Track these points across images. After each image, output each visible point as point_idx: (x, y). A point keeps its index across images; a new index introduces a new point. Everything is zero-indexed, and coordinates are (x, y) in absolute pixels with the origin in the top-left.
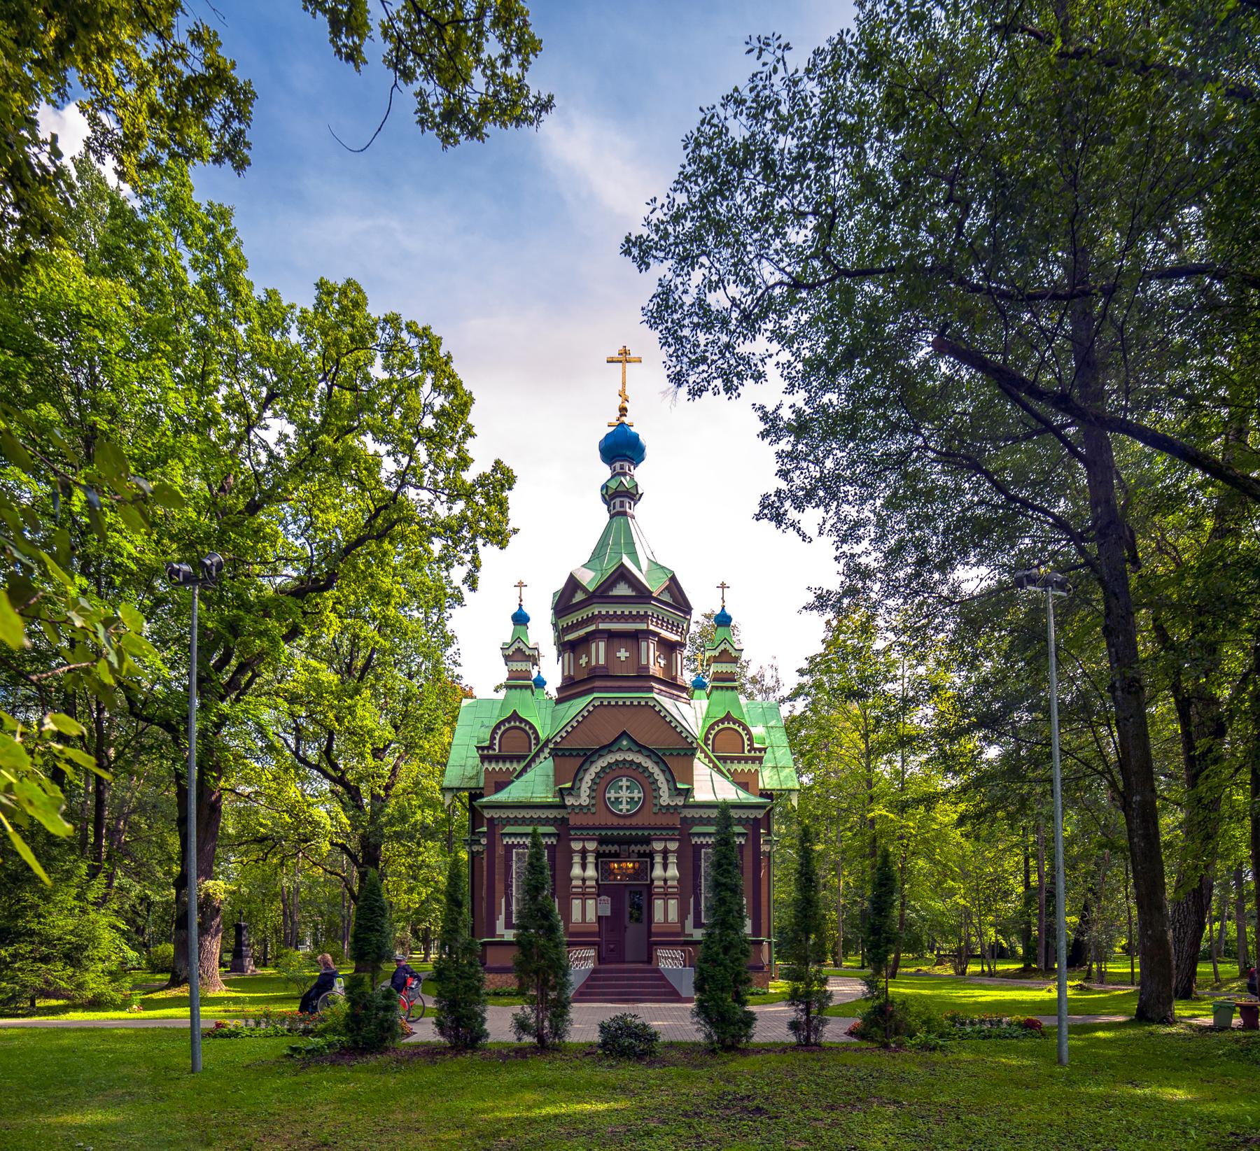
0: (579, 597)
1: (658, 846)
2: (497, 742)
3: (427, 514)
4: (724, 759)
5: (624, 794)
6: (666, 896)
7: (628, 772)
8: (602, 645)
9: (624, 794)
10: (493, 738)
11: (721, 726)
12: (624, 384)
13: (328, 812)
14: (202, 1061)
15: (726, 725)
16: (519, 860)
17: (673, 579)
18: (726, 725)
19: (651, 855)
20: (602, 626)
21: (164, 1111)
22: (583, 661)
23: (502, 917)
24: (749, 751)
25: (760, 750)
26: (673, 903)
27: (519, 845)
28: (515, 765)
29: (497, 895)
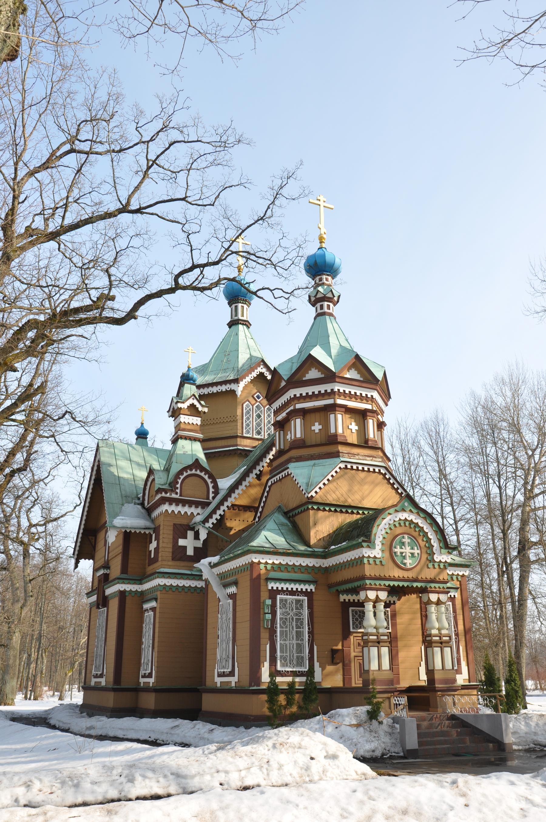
5: (407, 550)
7: (409, 531)
8: (298, 421)
9: (407, 550)
11: (189, 472)
12: (192, 6)
14: (267, 615)
15: (194, 472)
18: (194, 472)
19: (361, 604)
20: (298, 406)
23: (267, 664)
27: (282, 591)
28: (199, 510)
29: (263, 641)
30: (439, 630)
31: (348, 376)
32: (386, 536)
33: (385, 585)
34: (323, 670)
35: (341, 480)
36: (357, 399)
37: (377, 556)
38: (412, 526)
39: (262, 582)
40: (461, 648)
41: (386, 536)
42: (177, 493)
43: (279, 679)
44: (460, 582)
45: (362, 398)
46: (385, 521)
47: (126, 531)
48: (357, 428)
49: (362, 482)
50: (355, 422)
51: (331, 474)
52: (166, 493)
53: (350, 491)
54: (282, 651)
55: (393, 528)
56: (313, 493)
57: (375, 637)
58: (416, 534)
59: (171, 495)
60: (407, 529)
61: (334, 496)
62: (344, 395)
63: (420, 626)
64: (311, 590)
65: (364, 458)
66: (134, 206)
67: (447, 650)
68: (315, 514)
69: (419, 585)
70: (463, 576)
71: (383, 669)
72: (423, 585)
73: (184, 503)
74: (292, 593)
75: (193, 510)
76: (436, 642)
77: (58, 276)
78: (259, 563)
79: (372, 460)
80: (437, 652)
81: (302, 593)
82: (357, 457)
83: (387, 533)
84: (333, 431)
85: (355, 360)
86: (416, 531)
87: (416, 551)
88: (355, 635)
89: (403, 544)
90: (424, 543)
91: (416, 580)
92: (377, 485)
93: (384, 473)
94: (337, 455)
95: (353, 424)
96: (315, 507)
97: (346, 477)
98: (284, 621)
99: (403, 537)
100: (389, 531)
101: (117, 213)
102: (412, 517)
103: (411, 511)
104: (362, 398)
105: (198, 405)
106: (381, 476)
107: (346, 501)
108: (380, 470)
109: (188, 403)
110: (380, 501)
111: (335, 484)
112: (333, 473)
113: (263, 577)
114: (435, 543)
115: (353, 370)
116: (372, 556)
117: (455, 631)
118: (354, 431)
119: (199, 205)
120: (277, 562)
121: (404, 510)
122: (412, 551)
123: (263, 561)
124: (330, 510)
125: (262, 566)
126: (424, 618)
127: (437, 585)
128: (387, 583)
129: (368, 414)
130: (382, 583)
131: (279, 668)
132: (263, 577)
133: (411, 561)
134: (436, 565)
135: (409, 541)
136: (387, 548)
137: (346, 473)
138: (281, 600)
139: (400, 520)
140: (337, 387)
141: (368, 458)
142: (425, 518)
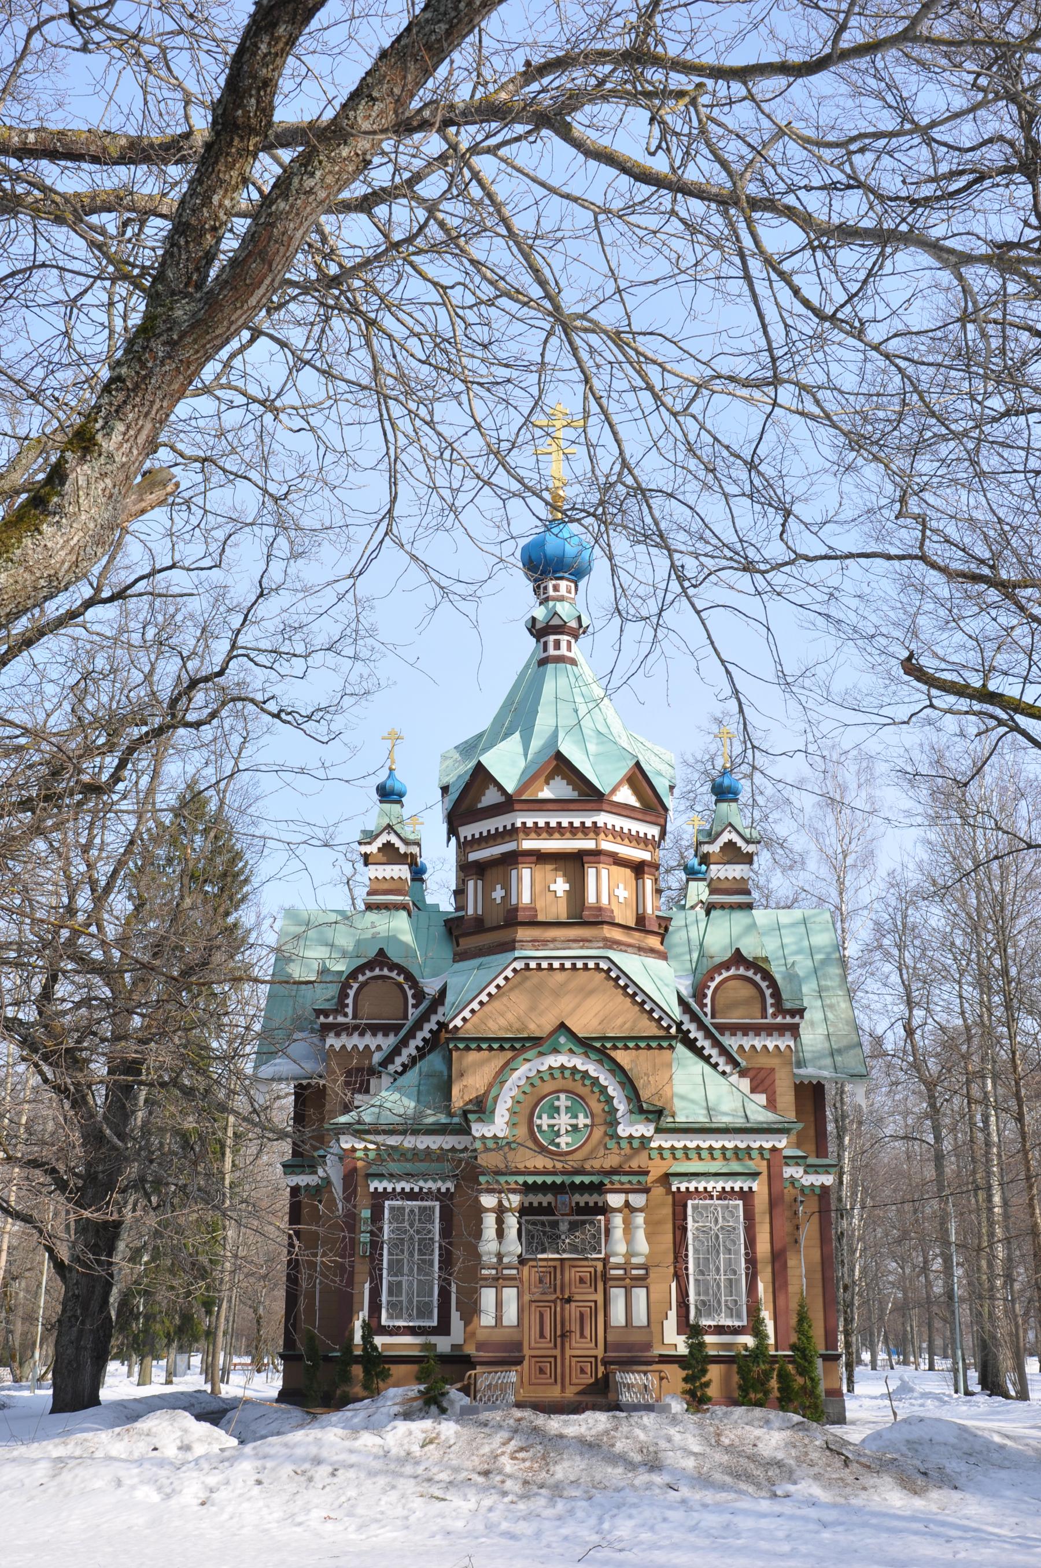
0: (491, 797)
1: (615, 1200)
2: (350, 1001)
4: (722, 1028)
5: (563, 1121)
6: (498, 1282)
9: (563, 1121)
10: (343, 995)
15: (377, 972)
17: (638, 764)
18: (377, 972)
21: (1009, 1279)
22: (498, 894)
23: (673, 1314)
26: (510, 1294)
27: (393, 1195)
31: (546, 794)
32: (521, 1098)
33: (516, 1182)
34: (465, 1326)
35: (517, 991)
36: (562, 835)
37: (501, 1135)
38: (578, 1077)
39: (360, 1180)
40: (761, 1286)
41: (521, 1098)
42: (346, 1015)
43: (379, 1341)
44: (768, 1160)
45: (573, 831)
46: (516, 1074)
47: (802, 1083)
48: (567, 887)
49: (557, 993)
50: (564, 875)
51: (495, 983)
52: (327, 1016)
53: (533, 1008)
54: (390, 1293)
55: (537, 1082)
56: (458, 1022)
57: (621, 1272)
58: (581, 1090)
59: (335, 1018)
60: (560, 1083)
61: (502, 1022)
62: (537, 831)
63: (671, 1246)
64: (448, 1189)
65: (566, 945)
66: (106, 594)
68: (460, 1059)
69: (587, 1180)
70: (774, 1149)
71: (505, 1323)
72: (596, 1179)
73: (362, 1031)
74: (411, 1196)
75: (370, 1041)
78: (354, 1150)
79: (582, 948)
80: (617, 1296)
81: (429, 1195)
82: (551, 945)
83: (524, 1093)
84: (514, 901)
85: (555, 763)
86: (584, 1085)
87: (582, 1121)
88: (531, 1263)
89: (557, 1109)
90: (602, 1105)
92: (591, 992)
93: (606, 968)
94: (509, 946)
95: (560, 880)
96: (461, 1046)
97: (528, 984)
98: (396, 1245)
99: (558, 1099)
100: (528, 1089)
101: (82, 610)
102: (578, 1062)
103: (571, 1051)
104: (573, 831)
106: (603, 975)
107: (525, 1028)
108: (597, 965)
109: (379, 843)
110: (595, 1022)
111: (505, 1000)
112: (500, 981)
113: (361, 1173)
114: (621, 1106)
115: (558, 779)
116: (489, 1135)
117: (747, 1254)
118: (560, 893)
119: (202, 569)
121: (556, 1051)
122: (574, 1121)
124: (491, 1049)
125: (360, 1154)
126: (678, 1232)
127: (625, 1179)
128: (521, 1179)
129: (586, 859)
130: (511, 1179)
131: (384, 1321)
132: (361, 1173)
133: (569, 1140)
134: (624, 1144)
135: (569, 1103)
137: (527, 978)
138: (392, 1209)
139: (550, 1068)
140: (520, 820)
141: (575, 945)
142: (600, 1062)
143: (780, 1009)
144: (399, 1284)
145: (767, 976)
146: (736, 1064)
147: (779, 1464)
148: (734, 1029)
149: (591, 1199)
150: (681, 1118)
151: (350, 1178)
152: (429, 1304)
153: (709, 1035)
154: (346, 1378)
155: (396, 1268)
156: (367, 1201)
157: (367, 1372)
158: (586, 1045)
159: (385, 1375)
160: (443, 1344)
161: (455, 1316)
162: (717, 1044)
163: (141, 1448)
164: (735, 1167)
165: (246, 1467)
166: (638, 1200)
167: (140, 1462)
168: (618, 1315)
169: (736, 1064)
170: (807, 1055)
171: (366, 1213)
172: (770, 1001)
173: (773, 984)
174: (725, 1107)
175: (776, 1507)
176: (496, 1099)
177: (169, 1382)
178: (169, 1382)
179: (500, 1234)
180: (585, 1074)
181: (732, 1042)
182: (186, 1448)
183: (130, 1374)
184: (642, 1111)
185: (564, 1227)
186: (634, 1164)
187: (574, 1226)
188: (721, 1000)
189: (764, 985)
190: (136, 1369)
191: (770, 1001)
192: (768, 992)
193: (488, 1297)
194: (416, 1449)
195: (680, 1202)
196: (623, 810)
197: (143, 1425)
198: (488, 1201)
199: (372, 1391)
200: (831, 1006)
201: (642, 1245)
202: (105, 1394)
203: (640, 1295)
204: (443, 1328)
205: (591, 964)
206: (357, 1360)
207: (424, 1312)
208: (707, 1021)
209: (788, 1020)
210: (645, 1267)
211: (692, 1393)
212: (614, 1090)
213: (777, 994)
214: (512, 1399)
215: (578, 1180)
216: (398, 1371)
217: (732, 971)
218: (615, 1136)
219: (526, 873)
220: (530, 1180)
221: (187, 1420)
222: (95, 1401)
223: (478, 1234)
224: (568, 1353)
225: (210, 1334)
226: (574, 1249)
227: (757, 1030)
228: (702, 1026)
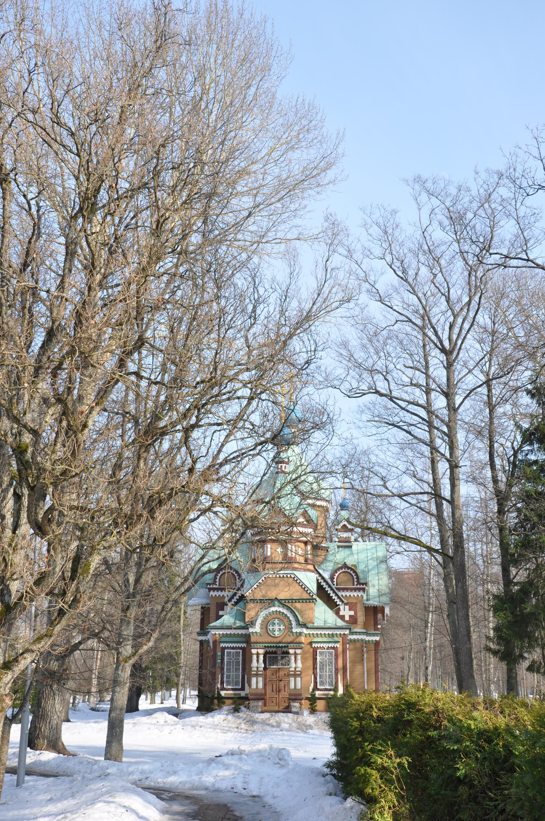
2: (217, 580)
3: (220, 220)
4: (339, 589)
6: (257, 675)
9: (277, 627)
13: (174, 592)
16: (228, 655)
24: (357, 585)
25: (363, 584)
26: (260, 679)
27: (228, 648)
30: (257, 668)
39: (218, 643)
40: (339, 676)
54: (227, 678)
56: (247, 594)
58: (281, 618)
67: (298, 679)
69: (283, 645)
70: (344, 634)
72: (286, 645)
74: (233, 648)
76: (292, 675)
77: (270, 451)
81: (239, 648)
87: (282, 627)
91: (280, 643)
98: (229, 663)
102: (281, 609)
105: (348, 525)
109: (342, 524)
114: (294, 623)
120: (221, 633)
121: (274, 606)
123: (217, 633)
125: (217, 636)
128: (264, 645)
130: (261, 645)
136: (264, 627)
143: (359, 583)
144: (230, 675)
145: (355, 572)
146: (343, 602)
147: (310, 726)
148: (344, 589)
149: (285, 650)
150: (316, 625)
151: (215, 642)
152: (238, 682)
153: (334, 592)
154: (212, 703)
155: (229, 670)
156: (220, 650)
157: (218, 702)
158: (282, 603)
159: (224, 703)
160: (243, 694)
161: (246, 685)
162: (337, 595)
163: (154, 721)
164: (331, 640)
165: (179, 726)
166: (298, 651)
167: (154, 724)
168: (292, 686)
169: (343, 602)
170: (371, 597)
171: (219, 654)
172: (355, 580)
173: (357, 574)
174: (329, 621)
175: (306, 735)
176: (256, 620)
177: (162, 703)
178: (162, 703)
179: (258, 661)
180: (283, 613)
181: (340, 594)
182: (166, 722)
183: (146, 699)
184: (300, 624)
185: (279, 658)
186: (298, 640)
187: (282, 658)
188: (339, 581)
189: (354, 574)
190: (149, 696)
191: (355, 580)
192: (355, 577)
193: (254, 680)
194: (221, 722)
195: (315, 650)
196: (302, 525)
197: (154, 716)
198: (254, 651)
199: (220, 707)
200: (381, 579)
201: (299, 664)
202: (140, 707)
203: (298, 679)
204: (243, 689)
205: (289, 576)
206: (216, 698)
207: (237, 683)
208: (334, 587)
209: (361, 586)
210: (300, 671)
211: (312, 709)
212: (292, 618)
213: (358, 578)
214: (260, 710)
215: (281, 645)
216: (227, 701)
217: (343, 570)
218: (292, 632)
219: (269, 546)
220: (266, 645)
221: (166, 714)
222: (137, 709)
223: (251, 661)
224: (280, 696)
225: (177, 684)
226: (282, 665)
227: (351, 590)
228: (332, 589)
